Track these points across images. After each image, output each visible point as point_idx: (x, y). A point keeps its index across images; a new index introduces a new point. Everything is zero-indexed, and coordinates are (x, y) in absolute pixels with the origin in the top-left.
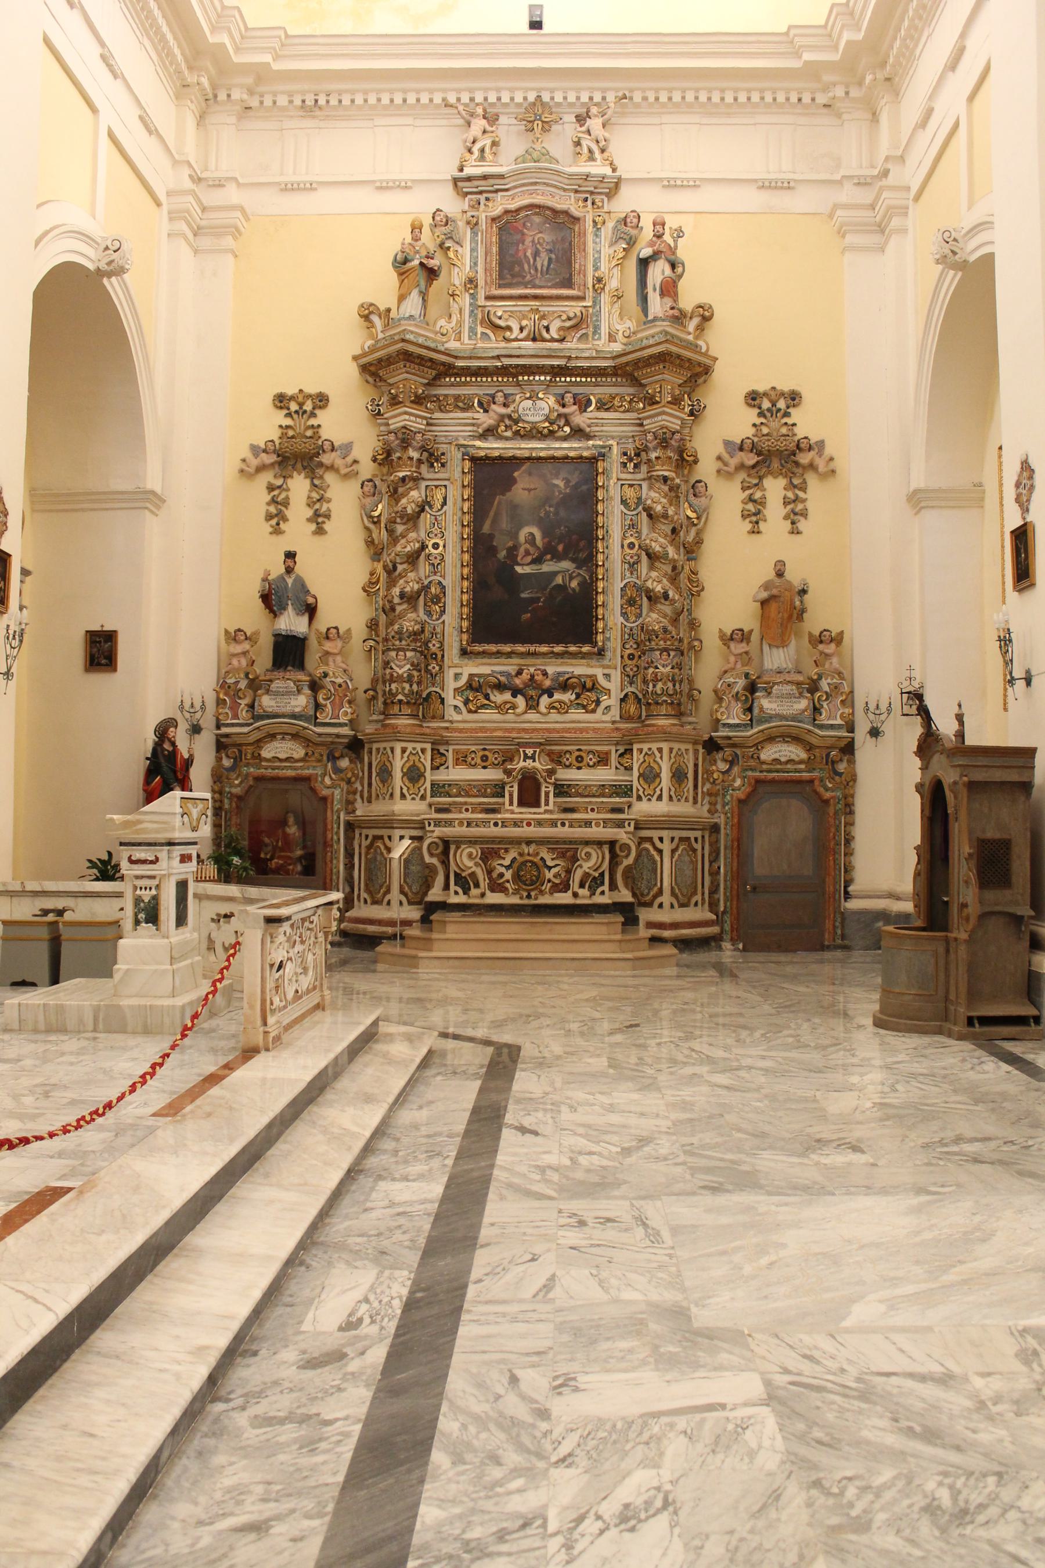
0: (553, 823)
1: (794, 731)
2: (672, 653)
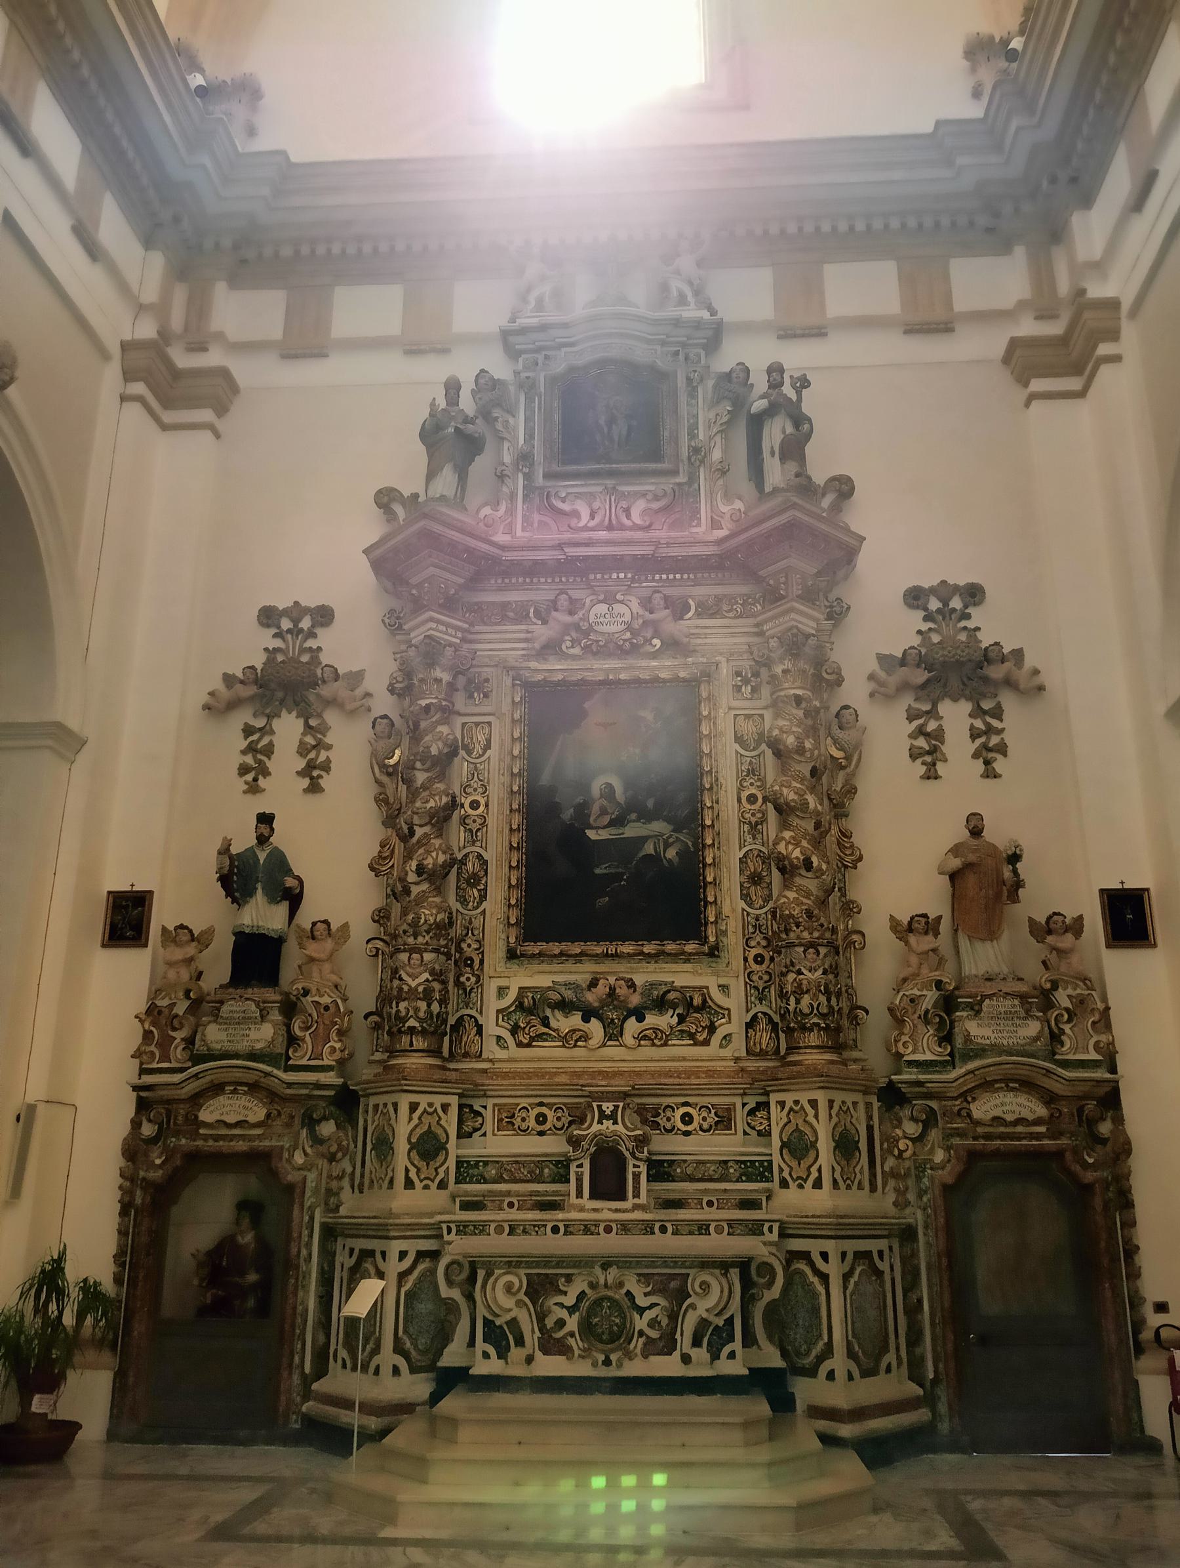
0: (648, 1228)
1: (1023, 1072)
2: (823, 950)
